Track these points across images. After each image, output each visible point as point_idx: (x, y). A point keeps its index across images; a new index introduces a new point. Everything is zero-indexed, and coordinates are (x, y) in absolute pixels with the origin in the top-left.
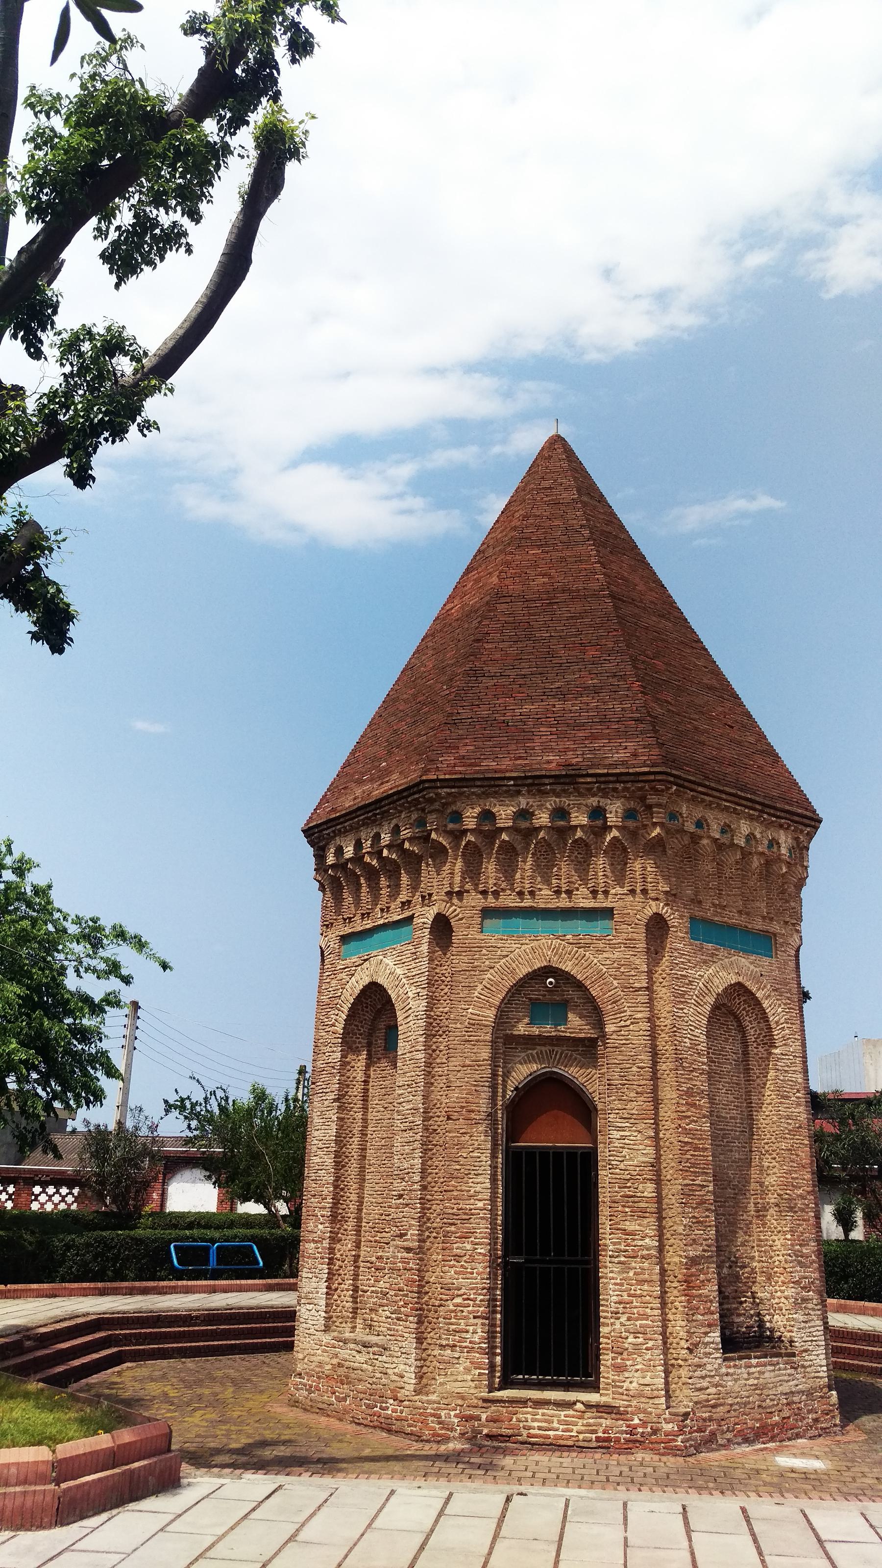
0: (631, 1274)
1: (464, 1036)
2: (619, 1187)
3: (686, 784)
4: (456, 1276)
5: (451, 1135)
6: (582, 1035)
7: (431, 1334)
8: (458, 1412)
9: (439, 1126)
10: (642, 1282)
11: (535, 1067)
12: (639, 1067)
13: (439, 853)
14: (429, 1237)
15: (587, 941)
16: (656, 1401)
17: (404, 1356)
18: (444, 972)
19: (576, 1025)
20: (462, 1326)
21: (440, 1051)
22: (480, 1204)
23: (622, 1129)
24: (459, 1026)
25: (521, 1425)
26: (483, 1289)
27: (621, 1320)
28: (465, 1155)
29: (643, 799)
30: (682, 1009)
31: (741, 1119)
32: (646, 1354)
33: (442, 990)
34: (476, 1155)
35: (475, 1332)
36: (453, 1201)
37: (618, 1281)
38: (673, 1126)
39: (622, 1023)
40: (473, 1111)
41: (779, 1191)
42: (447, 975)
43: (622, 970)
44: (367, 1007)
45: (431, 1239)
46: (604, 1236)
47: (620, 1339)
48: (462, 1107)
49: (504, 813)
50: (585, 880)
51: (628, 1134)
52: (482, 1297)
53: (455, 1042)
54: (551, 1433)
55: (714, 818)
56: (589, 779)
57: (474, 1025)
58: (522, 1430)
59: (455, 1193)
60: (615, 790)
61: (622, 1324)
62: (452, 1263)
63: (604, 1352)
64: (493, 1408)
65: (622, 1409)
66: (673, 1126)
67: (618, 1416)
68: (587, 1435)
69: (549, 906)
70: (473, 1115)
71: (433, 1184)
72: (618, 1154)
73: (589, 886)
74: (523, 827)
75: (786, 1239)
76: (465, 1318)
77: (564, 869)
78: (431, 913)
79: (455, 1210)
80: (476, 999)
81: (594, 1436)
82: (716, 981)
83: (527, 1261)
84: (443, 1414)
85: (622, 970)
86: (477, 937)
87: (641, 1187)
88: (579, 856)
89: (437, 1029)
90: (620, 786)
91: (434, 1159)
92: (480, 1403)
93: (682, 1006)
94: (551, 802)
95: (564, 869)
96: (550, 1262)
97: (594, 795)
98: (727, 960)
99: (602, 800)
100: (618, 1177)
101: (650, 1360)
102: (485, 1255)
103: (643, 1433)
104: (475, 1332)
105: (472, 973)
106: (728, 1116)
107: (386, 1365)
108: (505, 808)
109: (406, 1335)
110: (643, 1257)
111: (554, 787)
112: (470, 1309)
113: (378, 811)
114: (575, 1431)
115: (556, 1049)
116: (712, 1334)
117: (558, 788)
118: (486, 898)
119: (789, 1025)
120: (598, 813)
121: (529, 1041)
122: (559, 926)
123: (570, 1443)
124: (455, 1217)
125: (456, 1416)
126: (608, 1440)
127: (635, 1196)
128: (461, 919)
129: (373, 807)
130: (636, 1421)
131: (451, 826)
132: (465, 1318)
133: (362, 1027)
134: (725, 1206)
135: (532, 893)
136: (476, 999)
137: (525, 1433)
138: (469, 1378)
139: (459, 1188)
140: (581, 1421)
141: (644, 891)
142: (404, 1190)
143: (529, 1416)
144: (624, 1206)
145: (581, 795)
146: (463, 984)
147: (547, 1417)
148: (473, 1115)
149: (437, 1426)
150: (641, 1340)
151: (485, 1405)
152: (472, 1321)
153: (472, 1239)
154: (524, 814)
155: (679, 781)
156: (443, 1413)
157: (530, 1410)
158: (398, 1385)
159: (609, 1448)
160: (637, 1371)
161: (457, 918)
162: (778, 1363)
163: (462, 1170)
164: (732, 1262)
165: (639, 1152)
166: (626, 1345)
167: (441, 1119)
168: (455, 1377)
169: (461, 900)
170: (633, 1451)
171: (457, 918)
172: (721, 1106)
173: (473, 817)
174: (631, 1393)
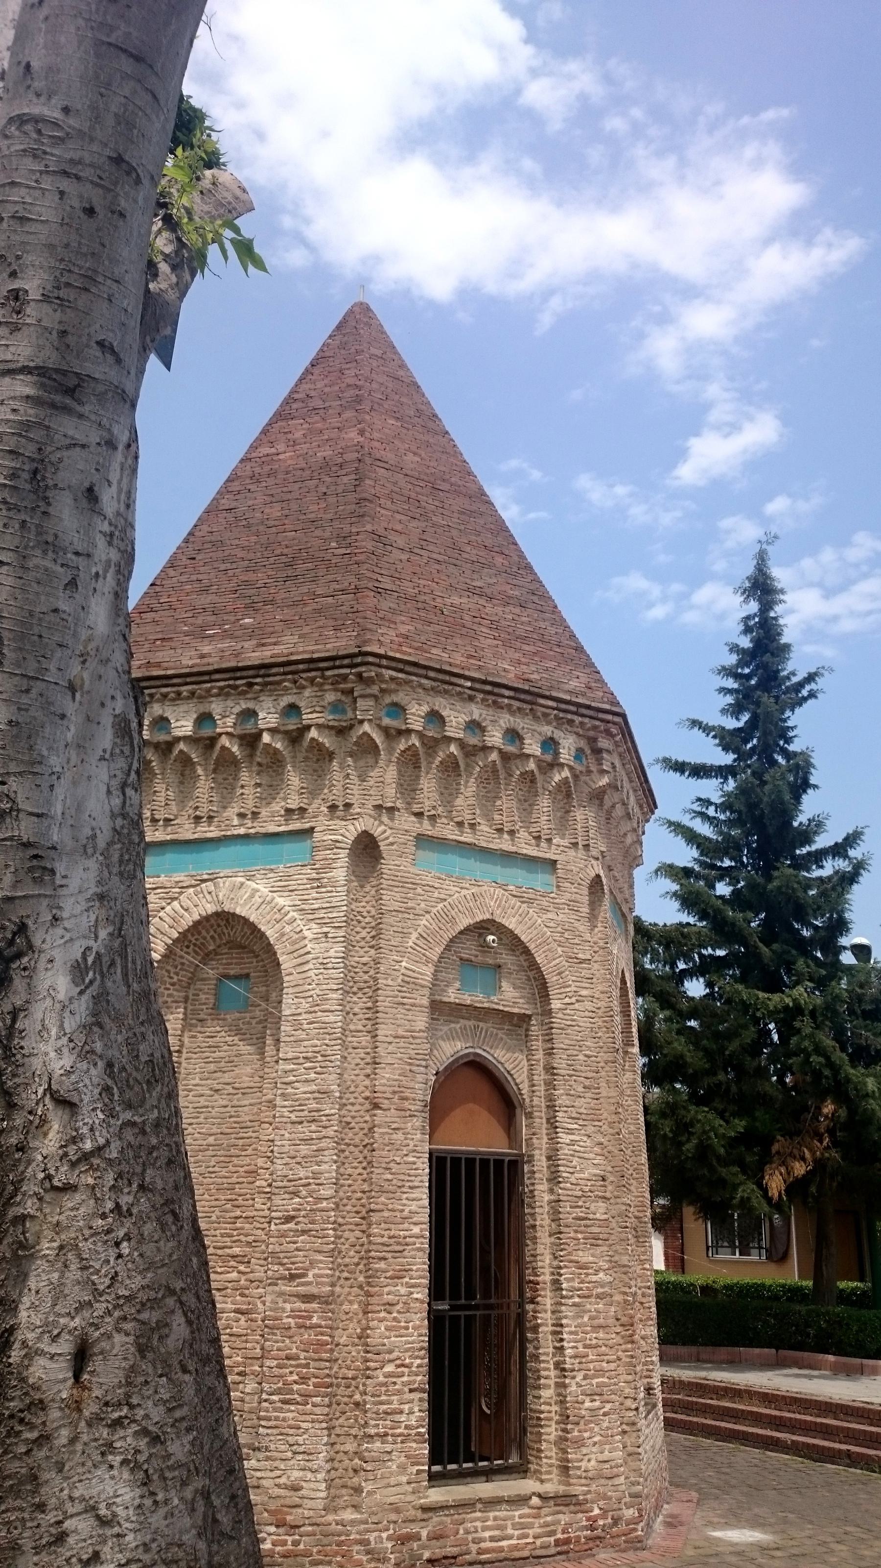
0: (586, 1319)
1: (396, 997)
4: (387, 1334)
5: (381, 1130)
6: (516, 1010)
7: (341, 1421)
8: (391, 1532)
9: (353, 1117)
10: (597, 1328)
11: (459, 1045)
12: (586, 1056)
13: (367, 749)
14: (339, 1278)
15: (530, 896)
16: (616, 1481)
17: (300, 1457)
18: (361, 910)
19: (510, 996)
21: (355, 1014)
22: (416, 1230)
23: (570, 1132)
24: (390, 982)
25: (470, 1537)
26: (421, 1349)
27: (577, 1379)
28: (398, 1159)
33: (357, 933)
34: (411, 1159)
35: (411, 1412)
36: (383, 1225)
37: (573, 1329)
38: (611, 1131)
39: (567, 1000)
40: (406, 1099)
41: (637, 1214)
42: (365, 914)
43: (566, 935)
44: (188, 947)
45: (342, 1281)
46: (542, 1270)
48: (394, 1092)
49: (456, 718)
50: (527, 823)
51: (578, 1138)
52: (419, 1361)
53: (386, 1004)
54: (504, 1543)
56: (550, 703)
57: (408, 983)
58: (471, 1545)
59: (386, 1214)
60: (571, 722)
61: (579, 1385)
62: (383, 1314)
63: (547, 1423)
64: (435, 1519)
65: (581, 1497)
66: (611, 1131)
67: (578, 1508)
68: (545, 1539)
69: (491, 846)
70: (406, 1104)
71: (345, 1201)
73: (531, 830)
74: (471, 743)
75: (644, 1269)
76: (399, 1392)
77: (507, 803)
78: (350, 831)
79: (385, 1239)
80: (410, 950)
81: (552, 1539)
83: (453, 1308)
84: (372, 1539)
85: (566, 935)
86: (411, 870)
87: (593, 1208)
88: (520, 793)
89: (351, 984)
90: (578, 719)
91: (347, 1165)
92: (419, 1514)
94: (506, 720)
95: (507, 803)
96: (477, 1307)
97: (549, 723)
99: (556, 731)
100: (570, 1193)
101: (608, 1428)
102: (422, 1302)
103: (604, 1525)
104: (411, 1412)
105: (406, 916)
107: (259, 1474)
108: (456, 714)
109: (304, 1425)
110: (598, 1296)
111: (513, 702)
112: (405, 1379)
113: (258, 680)
114: (289, 1543)
115: (481, 1024)
117: (516, 704)
118: (421, 823)
120: (550, 744)
121: (458, 1011)
122: (499, 872)
123: (526, 1553)
124: (386, 1248)
125: (389, 1538)
126: (567, 1541)
127: (586, 1219)
128: (392, 844)
129: (251, 673)
130: (596, 1511)
131: (386, 721)
132: (399, 1392)
133: (177, 974)
135: (472, 826)
136: (410, 950)
137: (474, 1548)
138: (404, 1479)
139: (390, 1206)
140: (537, 1521)
141: (586, 846)
142: (299, 1210)
143: (479, 1524)
144: (576, 1232)
145: (536, 718)
146: (395, 929)
147: (500, 1522)
148: (406, 1104)
149: (365, 1558)
150: (597, 1404)
151: (425, 1516)
152: (408, 1396)
153: (407, 1279)
154: (474, 726)
156: (372, 1537)
157: (478, 1514)
158: (288, 1502)
159: (567, 1552)
161: (387, 842)
163: (395, 1182)
165: (589, 1162)
166: (583, 1412)
167: (357, 1107)
168: (386, 1481)
169: (392, 819)
170: (594, 1551)
171: (387, 842)
173: (419, 716)
174: (590, 1474)
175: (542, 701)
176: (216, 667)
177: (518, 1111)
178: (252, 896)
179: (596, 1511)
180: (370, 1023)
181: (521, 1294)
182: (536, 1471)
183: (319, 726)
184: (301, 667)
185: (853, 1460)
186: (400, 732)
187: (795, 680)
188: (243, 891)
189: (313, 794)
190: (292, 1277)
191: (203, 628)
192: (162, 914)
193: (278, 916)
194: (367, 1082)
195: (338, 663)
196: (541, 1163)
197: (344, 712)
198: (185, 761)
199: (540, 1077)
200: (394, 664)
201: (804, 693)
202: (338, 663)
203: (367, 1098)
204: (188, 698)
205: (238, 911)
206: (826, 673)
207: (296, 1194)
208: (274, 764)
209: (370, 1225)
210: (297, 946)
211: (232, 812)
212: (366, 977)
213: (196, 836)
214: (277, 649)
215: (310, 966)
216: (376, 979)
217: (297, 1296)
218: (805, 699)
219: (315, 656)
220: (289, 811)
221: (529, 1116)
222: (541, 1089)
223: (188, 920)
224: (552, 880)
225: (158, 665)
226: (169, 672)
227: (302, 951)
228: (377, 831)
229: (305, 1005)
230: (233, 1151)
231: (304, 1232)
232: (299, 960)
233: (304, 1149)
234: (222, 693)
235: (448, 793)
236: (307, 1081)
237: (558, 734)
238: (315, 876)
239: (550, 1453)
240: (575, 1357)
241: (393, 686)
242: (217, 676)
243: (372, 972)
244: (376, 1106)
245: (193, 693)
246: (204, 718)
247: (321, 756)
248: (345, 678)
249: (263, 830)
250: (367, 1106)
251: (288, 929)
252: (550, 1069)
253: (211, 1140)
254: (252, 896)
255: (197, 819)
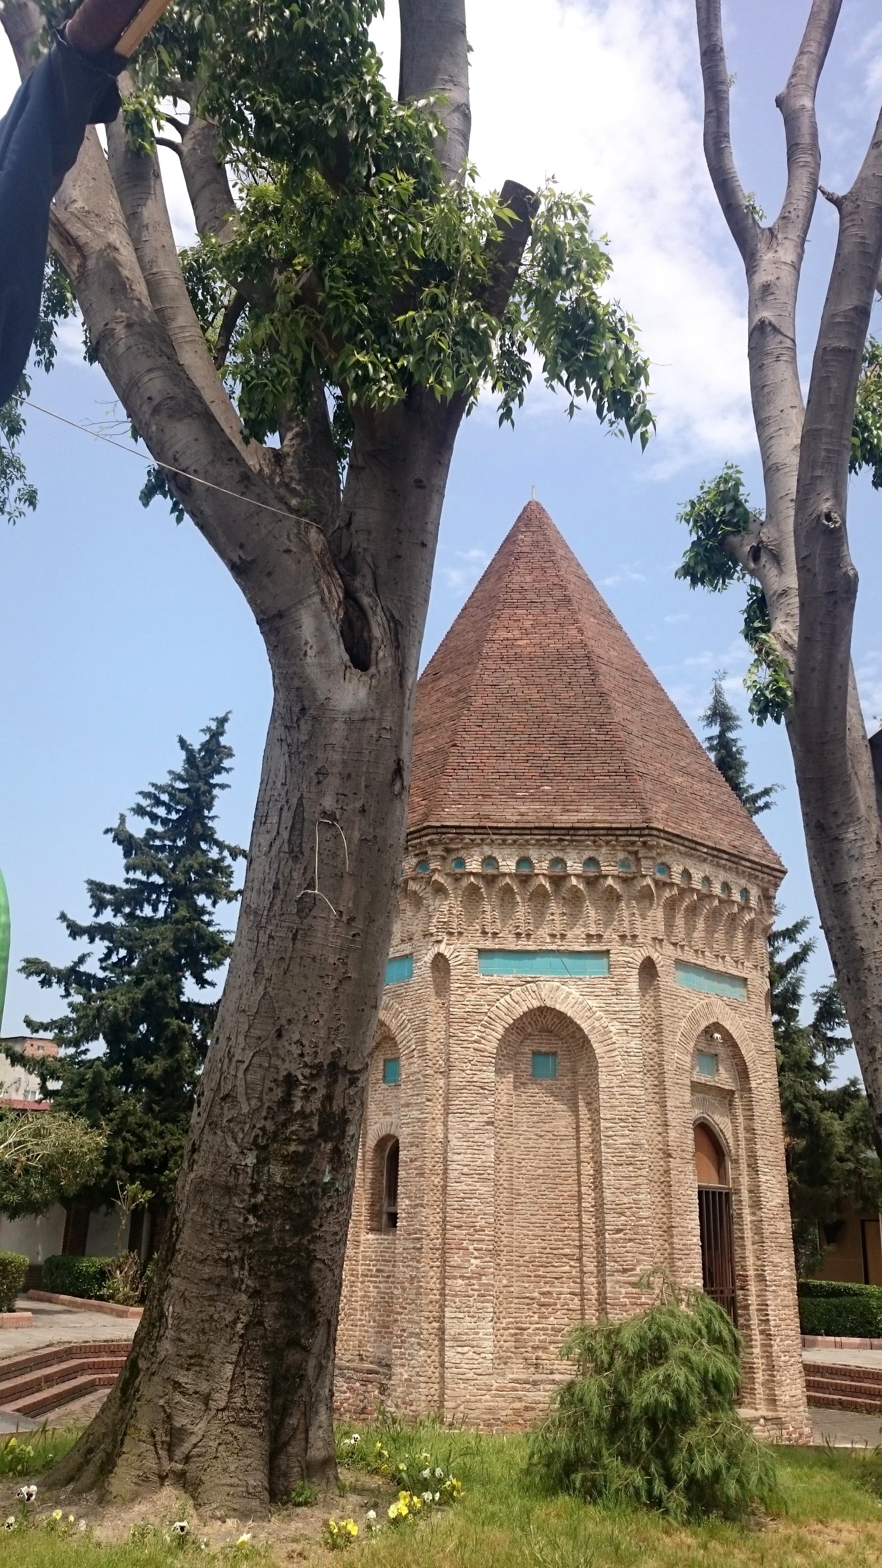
6: (727, 1087)
13: (646, 896)
19: (724, 1078)
23: (765, 1173)
56: (748, 864)
78: (639, 955)
113: (568, 838)
120: (745, 892)
129: (563, 832)
131: (658, 876)
167: (654, 1156)
175: (744, 863)
176: (537, 825)
177: (727, 1158)
178: (567, 997)
179: (791, 1429)
180: (657, 1096)
181: (733, 1284)
182: (749, 1403)
183: (613, 876)
184: (602, 832)
185: (843, 1406)
186: (665, 884)
187: (752, 792)
188: (559, 993)
189: (607, 924)
190: (625, 1271)
191: (514, 789)
192: (497, 1004)
193: (588, 1014)
194: (659, 1138)
195: (630, 832)
196: (745, 1195)
197: (629, 867)
198: (508, 889)
199: (742, 1135)
200: (667, 836)
201: (760, 803)
202: (630, 832)
203: (660, 1149)
204: (510, 845)
205: (558, 1007)
206: (779, 789)
207: (622, 1214)
208: (575, 900)
209: (672, 1237)
210: (606, 1037)
211: (544, 932)
212: (652, 1063)
213: (519, 948)
214: (581, 816)
215: (616, 1053)
216: (660, 1065)
217: (629, 1283)
218: (761, 809)
219: (614, 826)
220: (589, 936)
221: (736, 1161)
222: (743, 1144)
223: (520, 1010)
224: (743, 991)
225: (487, 817)
226: (500, 825)
227: (609, 1042)
228: (655, 956)
229: (616, 1081)
230: (558, 1181)
231: (630, 1240)
232: (608, 1048)
233: (625, 1184)
234: (539, 844)
235: (690, 928)
236: (623, 1136)
237: (749, 886)
238: (613, 986)
239: (760, 1391)
240: (775, 1326)
241: (664, 851)
242: (536, 832)
243: (656, 1060)
244: (670, 1156)
245: (515, 841)
246: (524, 861)
247: (613, 898)
248: (633, 843)
249: (570, 948)
250: (661, 1155)
251: (597, 1024)
252: (750, 1130)
253: (540, 1171)
254: (567, 997)
255: (518, 935)
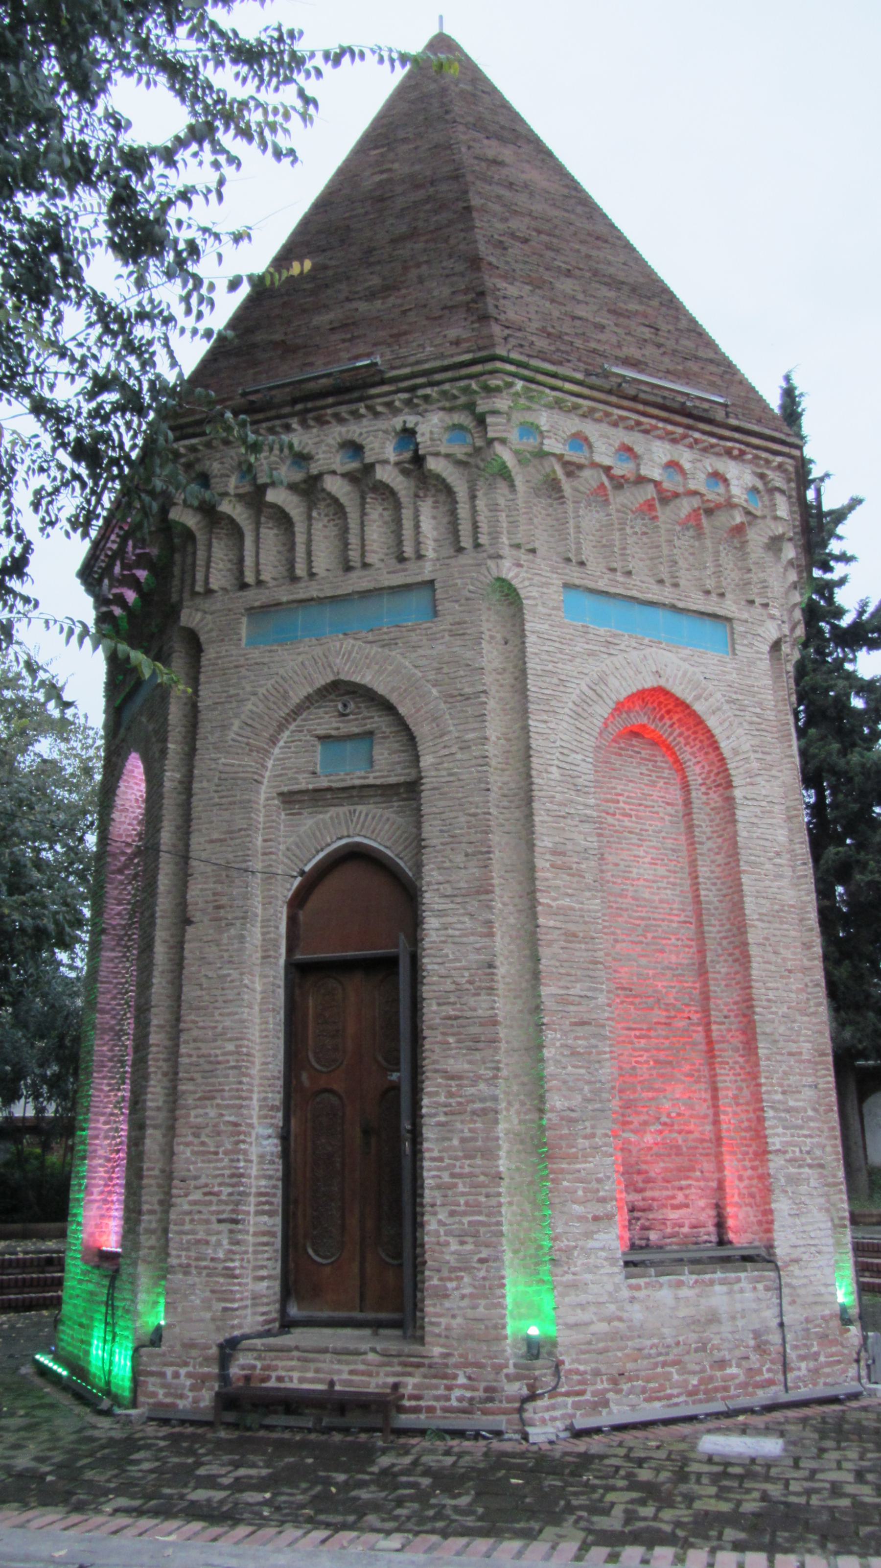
2: (439, 1004)
3: (541, 378)
20: (201, 1235)
29: (470, 407)
30: (545, 722)
31: (682, 903)
32: (479, 1270)
47: (437, 1248)
55: (601, 436)
72: (439, 953)
76: (207, 1222)
79: (194, 1059)
82: (613, 682)
85: (445, 670)
93: (545, 717)
98: (635, 653)
101: (484, 1278)
106: (656, 898)
110: (474, 1113)
116: (601, 1236)
119: (760, 756)
132: (207, 1222)
134: (649, 1037)
139: (201, 1024)
145: (376, 415)
150: (469, 1247)
152: (216, 1226)
155: (526, 373)
160: (463, 1297)
162: (739, 1280)
164: (665, 1124)
172: (641, 882)
